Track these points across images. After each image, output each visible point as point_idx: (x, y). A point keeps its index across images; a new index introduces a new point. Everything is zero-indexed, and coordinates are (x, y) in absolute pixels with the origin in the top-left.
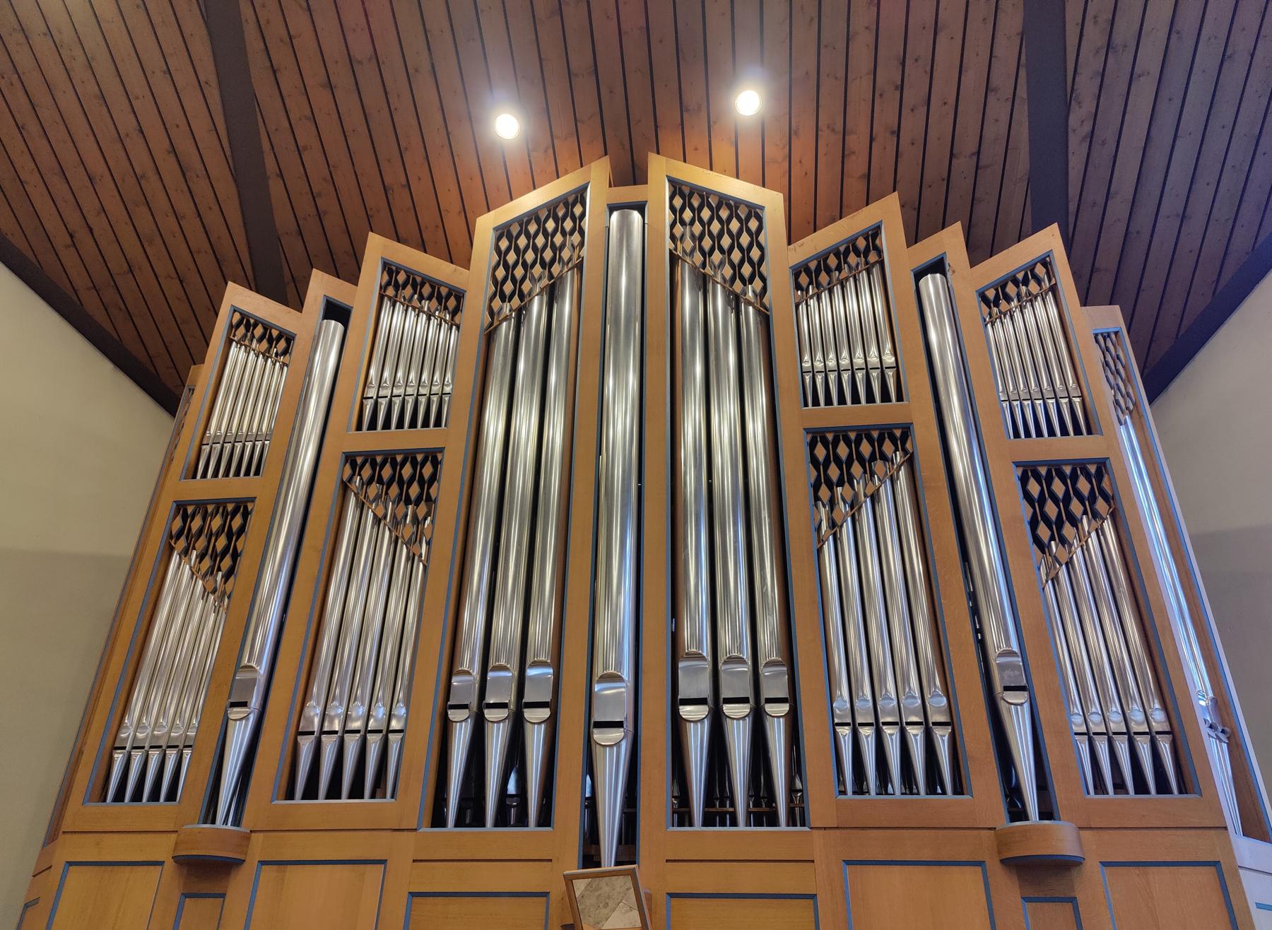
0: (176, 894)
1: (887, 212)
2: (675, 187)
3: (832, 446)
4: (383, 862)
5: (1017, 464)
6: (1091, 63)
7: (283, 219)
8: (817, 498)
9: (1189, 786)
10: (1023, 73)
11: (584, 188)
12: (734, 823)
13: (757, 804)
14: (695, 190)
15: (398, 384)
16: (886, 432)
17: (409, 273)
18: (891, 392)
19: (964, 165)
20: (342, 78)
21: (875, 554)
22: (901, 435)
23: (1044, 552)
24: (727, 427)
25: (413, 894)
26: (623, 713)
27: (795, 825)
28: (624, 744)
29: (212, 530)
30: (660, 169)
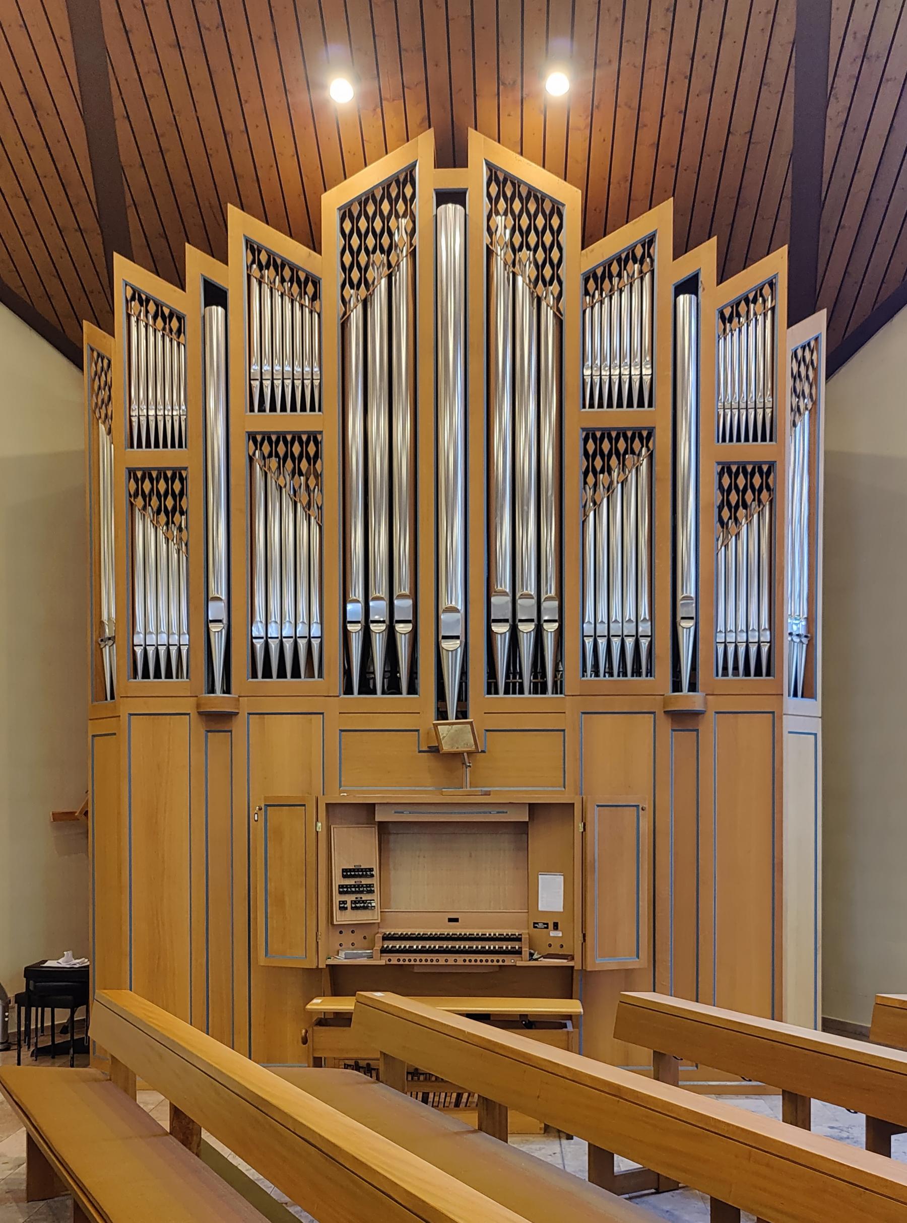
0: (203, 732)
1: (660, 220)
2: (491, 171)
3: (598, 442)
4: (322, 713)
5: (719, 463)
6: (848, 68)
7: (127, 153)
8: (585, 483)
9: (772, 671)
10: (792, 71)
11: (413, 166)
12: (521, 692)
13: (535, 677)
14: (508, 178)
15: (281, 370)
16: (637, 433)
17: (269, 253)
18: (643, 398)
19: (738, 141)
20: (189, 39)
21: (618, 522)
22: (646, 436)
23: (723, 527)
24: (527, 438)
25: (342, 731)
26: (459, 631)
27: (557, 693)
28: (459, 650)
29: (162, 493)
30: (480, 148)
